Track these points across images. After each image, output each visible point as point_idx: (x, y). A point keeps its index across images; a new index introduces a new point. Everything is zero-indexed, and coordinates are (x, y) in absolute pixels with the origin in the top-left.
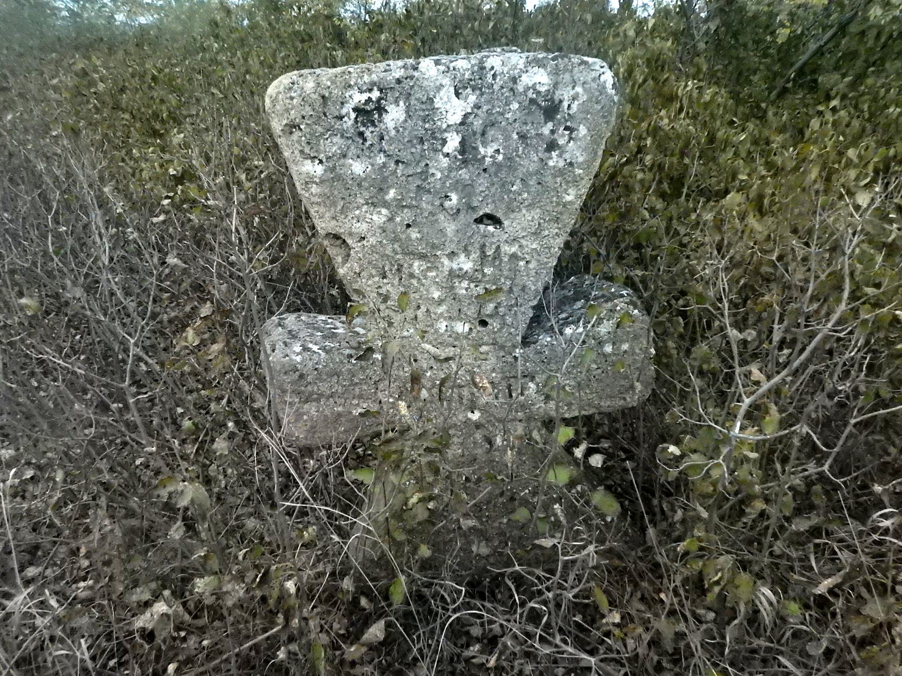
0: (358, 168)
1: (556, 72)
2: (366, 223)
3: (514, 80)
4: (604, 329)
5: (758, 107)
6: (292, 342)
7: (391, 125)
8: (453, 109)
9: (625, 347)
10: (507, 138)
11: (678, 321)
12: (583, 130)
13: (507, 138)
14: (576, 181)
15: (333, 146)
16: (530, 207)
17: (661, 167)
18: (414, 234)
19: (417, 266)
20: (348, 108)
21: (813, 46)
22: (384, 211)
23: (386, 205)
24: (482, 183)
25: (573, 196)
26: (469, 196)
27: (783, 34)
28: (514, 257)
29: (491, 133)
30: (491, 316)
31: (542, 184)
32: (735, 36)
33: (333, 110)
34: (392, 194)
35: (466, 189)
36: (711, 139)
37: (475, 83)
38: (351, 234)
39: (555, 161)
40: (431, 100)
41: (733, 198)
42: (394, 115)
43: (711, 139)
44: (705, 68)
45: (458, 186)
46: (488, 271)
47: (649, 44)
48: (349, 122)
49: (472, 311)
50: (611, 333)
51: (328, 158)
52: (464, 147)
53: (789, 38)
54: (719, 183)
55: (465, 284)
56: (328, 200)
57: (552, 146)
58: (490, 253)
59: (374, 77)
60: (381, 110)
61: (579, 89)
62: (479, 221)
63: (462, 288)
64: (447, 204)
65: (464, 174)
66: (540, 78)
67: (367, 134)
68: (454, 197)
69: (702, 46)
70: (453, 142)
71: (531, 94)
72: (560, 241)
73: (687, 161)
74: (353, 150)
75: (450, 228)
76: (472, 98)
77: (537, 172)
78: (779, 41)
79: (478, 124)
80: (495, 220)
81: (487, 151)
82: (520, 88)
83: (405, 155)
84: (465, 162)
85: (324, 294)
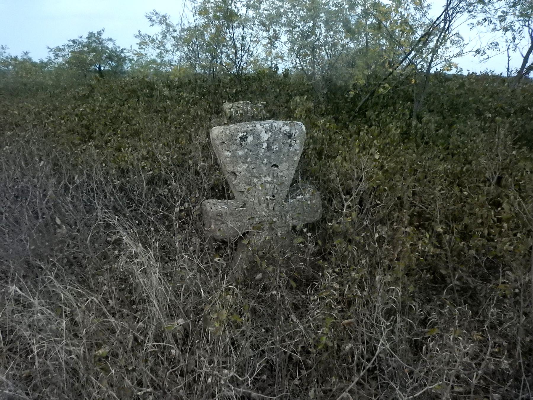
0: (240, 153)
1: (291, 126)
2: (241, 168)
3: (281, 129)
4: (307, 196)
5: (346, 124)
6: (214, 206)
7: (249, 141)
8: (265, 137)
9: (314, 201)
10: (279, 144)
11: (328, 195)
12: (298, 141)
13: (279, 144)
14: (297, 155)
15: (234, 147)
16: (286, 162)
17: (315, 149)
18: (255, 171)
19: (255, 180)
20: (238, 137)
21: (364, 99)
22: (246, 165)
23: (247, 163)
24: (273, 156)
25: (297, 158)
26: (270, 159)
27: (352, 93)
28: (282, 176)
29: (275, 142)
30: (276, 194)
31: (288, 155)
32: (334, 94)
33: (234, 138)
34: (249, 159)
35: (268, 157)
36: (330, 139)
37: (271, 129)
38: (237, 172)
39: (292, 149)
40: (260, 135)
41: (339, 158)
42: (250, 139)
43: (330, 139)
44: (324, 109)
45: (267, 157)
46: (275, 180)
47: (305, 104)
48: (238, 141)
49: (270, 193)
50: (309, 196)
51: (232, 151)
52: (268, 147)
53: (354, 95)
54: (334, 153)
55: (268, 185)
56: (232, 162)
57: (291, 145)
58: (275, 175)
59: (245, 129)
60: (246, 137)
61: (297, 131)
62: (272, 166)
63: (268, 186)
64: (264, 162)
65: (268, 153)
66: (287, 128)
67: (243, 144)
68: (266, 160)
69: (322, 99)
70: (265, 145)
71: (285, 132)
72: (294, 171)
73: (323, 146)
74: (239, 149)
75: (265, 169)
76: (270, 134)
77: (287, 152)
78: (351, 96)
79: (271, 140)
80: (275, 166)
81: (274, 147)
82: (282, 131)
83: (252, 149)
84: (268, 150)
85: (221, 191)
